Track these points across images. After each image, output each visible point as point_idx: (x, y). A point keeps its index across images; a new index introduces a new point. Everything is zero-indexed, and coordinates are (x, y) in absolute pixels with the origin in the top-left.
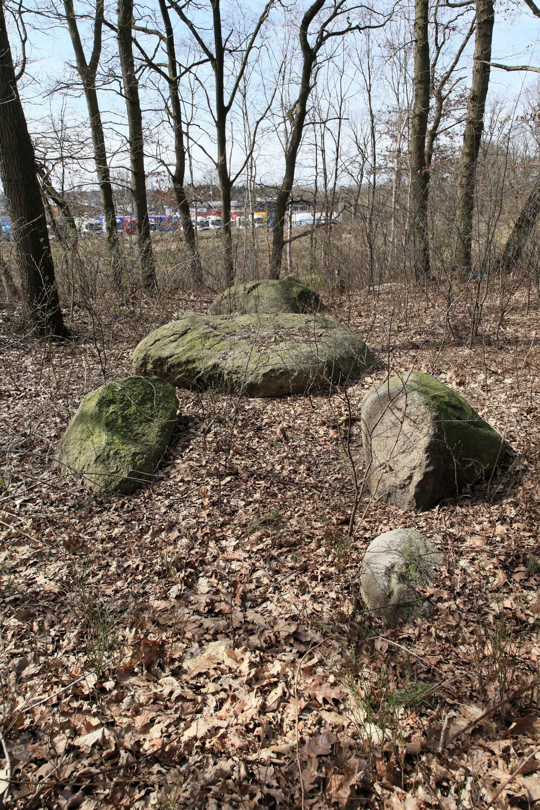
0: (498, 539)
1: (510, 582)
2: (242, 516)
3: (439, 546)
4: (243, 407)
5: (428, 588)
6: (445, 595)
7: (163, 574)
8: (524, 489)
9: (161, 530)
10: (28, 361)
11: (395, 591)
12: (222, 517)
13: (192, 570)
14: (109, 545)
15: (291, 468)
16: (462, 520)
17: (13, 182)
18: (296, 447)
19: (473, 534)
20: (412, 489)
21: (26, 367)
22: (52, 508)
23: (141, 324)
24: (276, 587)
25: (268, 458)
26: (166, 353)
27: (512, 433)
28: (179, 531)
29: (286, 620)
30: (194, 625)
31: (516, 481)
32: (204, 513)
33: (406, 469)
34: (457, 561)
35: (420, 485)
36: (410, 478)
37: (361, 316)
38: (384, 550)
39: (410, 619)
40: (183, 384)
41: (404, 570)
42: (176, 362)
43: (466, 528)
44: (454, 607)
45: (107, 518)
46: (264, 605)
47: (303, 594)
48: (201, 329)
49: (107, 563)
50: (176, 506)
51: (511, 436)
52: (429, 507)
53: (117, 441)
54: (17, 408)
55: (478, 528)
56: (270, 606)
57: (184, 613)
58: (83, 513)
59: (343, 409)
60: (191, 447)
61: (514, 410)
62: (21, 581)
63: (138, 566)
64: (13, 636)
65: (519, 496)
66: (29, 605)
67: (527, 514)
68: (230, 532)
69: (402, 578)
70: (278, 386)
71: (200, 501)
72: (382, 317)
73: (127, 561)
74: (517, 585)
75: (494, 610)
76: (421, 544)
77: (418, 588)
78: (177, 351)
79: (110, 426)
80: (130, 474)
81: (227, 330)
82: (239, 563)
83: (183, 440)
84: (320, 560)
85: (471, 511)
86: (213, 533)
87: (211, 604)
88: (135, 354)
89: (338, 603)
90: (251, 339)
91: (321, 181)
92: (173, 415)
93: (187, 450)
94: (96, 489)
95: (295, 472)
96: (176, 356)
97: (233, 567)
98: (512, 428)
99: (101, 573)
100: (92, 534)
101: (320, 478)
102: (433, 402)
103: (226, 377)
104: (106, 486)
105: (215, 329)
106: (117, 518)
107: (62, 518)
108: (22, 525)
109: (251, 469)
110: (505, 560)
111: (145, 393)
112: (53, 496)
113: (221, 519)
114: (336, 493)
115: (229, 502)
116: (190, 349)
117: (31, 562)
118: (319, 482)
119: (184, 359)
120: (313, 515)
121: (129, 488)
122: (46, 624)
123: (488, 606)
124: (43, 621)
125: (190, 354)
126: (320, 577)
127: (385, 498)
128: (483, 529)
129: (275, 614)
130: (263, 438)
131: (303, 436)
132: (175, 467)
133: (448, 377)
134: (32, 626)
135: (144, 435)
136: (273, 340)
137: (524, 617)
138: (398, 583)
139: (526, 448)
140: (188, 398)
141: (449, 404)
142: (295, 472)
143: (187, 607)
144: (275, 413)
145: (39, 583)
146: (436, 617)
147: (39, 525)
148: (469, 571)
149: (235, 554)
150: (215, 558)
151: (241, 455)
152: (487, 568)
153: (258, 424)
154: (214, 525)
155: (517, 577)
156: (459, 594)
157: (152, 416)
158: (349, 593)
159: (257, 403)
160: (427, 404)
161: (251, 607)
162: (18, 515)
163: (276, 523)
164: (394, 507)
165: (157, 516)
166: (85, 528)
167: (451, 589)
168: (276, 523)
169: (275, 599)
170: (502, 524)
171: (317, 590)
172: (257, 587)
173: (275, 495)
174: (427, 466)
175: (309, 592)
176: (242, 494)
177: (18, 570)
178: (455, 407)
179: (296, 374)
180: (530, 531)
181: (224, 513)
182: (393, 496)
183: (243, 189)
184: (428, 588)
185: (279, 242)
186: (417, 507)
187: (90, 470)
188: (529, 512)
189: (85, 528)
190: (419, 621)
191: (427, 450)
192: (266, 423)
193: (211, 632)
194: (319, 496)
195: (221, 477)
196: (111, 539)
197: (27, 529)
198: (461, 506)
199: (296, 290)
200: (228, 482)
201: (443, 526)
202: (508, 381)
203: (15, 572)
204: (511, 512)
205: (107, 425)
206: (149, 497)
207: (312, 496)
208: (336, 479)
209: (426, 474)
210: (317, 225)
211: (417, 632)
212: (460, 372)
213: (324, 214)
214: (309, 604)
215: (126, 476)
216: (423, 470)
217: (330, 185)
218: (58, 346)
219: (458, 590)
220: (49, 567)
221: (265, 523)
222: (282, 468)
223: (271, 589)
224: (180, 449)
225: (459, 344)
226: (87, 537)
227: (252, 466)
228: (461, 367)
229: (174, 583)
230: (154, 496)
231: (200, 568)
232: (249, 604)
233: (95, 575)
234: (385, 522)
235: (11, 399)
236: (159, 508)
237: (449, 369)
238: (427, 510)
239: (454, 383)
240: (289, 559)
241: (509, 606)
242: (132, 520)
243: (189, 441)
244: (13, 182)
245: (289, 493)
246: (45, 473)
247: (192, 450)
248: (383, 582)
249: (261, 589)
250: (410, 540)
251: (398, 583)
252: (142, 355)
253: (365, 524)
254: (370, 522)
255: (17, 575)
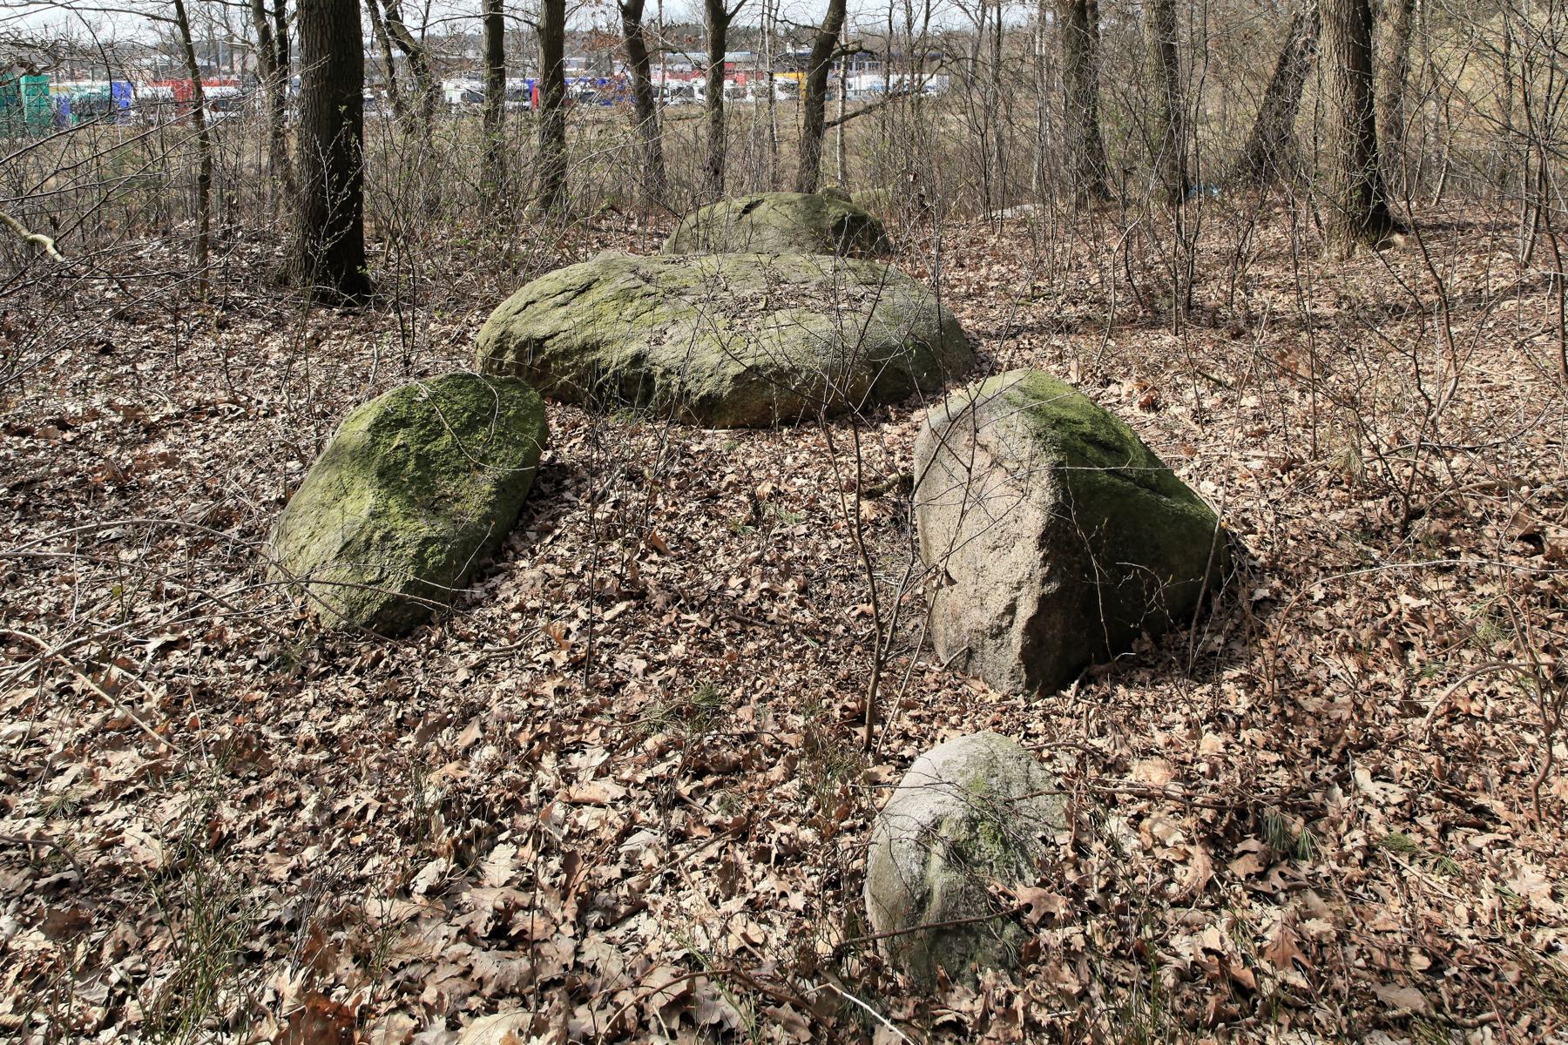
0: (1204, 767)
1: (1222, 880)
2: (634, 697)
3: (1060, 780)
4: (687, 447)
5: (1019, 886)
6: (1060, 907)
7: (414, 833)
8: (1273, 646)
9: (443, 723)
10: (274, 347)
11: (937, 889)
12: (588, 695)
13: (477, 822)
14: (316, 757)
15: (766, 585)
16: (1127, 719)
17: (316, 11)
18: (785, 538)
19: (1147, 753)
20: (1016, 637)
21: (266, 357)
22: (220, 664)
23: (512, 270)
24: (670, 876)
25: (720, 561)
26: (541, 330)
27: (1248, 515)
28: (483, 728)
29: (676, 963)
30: (455, 970)
31: (1249, 628)
32: (549, 687)
33: (1002, 588)
34: (1101, 821)
35: (1032, 626)
36: (1011, 609)
37: (962, 266)
38: (930, 787)
39: (966, 971)
40: (568, 397)
41: (963, 834)
42: (560, 347)
43: (1135, 740)
44: (1078, 942)
45: (333, 690)
46: (631, 923)
47: (728, 898)
48: (620, 280)
49: (298, 799)
50: (492, 667)
51: (1245, 521)
52: (1053, 687)
53: (395, 510)
54: (223, 439)
55: (1160, 739)
56: (644, 925)
57: (436, 937)
58: (283, 678)
59: (897, 458)
60: (557, 532)
61: (1256, 464)
62: (89, 836)
63: (365, 810)
64: (19, 979)
65: (1258, 662)
66: (75, 895)
67: (1274, 708)
68: (596, 733)
69: (958, 855)
70: (763, 402)
71: (548, 656)
72: (1004, 270)
73: (344, 795)
74: (1239, 889)
75: (1177, 955)
76: (1017, 773)
77: (996, 886)
78: (565, 326)
79: (388, 476)
80: (408, 587)
81: (672, 284)
82: (600, 812)
83: (545, 516)
84: (786, 807)
85: (1150, 697)
86: (557, 733)
87: (503, 916)
88: (485, 333)
89: (807, 923)
90: (712, 304)
91: (900, 18)
92: (532, 457)
93: (549, 539)
94: (328, 622)
95: (773, 595)
96: (562, 335)
97: (582, 821)
98: (1248, 504)
99: (275, 824)
100: (288, 728)
101: (826, 613)
102: (1052, 433)
103: (658, 381)
104: (351, 614)
105: (648, 281)
106: (355, 692)
107: (237, 685)
108: (141, 700)
109: (675, 586)
110: (1215, 821)
111: (478, 408)
112: (232, 635)
113: (584, 702)
114: (857, 648)
115: (611, 661)
116: (592, 322)
117: (130, 790)
118: (824, 620)
119: (577, 341)
120: (791, 699)
121: (399, 622)
122: (108, 950)
123: (1164, 945)
124: (102, 941)
125: (590, 330)
126: (775, 852)
127: (962, 660)
128: (1170, 743)
129: (653, 948)
130: (719, 516)
131: (803, 513)
132: (512, 577)
133: (1124, 392)
134: (70, 955)
135: (457, 500)
136: (761, 305)
137: (1247, 976)
138: (944, 870)
139: (1277, 548)
140: (575, 426)
141: (1090, 439)
142: (773, 595)
143: (448, 919)
144: (750, 462)
145: (127, 844)
146: (1032, 968)
147: (179, 703)
148: (1127, 849)
149: (593, 791)
150: (547, 796)
151: (660, 553)
152: (1170, 843)
153: (713, 485)
154: (565, 716)
155: (1240, 868)
156: (1095, 907)
157: (484, 458)
158: (837, 898)
159: (718, 438)
160: (1039, 436)
161: (601, 928)
162: (144, 676)
163: (705, 714)
164: (979, 685)
165: (445, 691)
166: (277, 713)
167: (1077, 892)
168: (705, 714)
169: (660, 908)
170: (1216, 731)
171: (763, 886)
172: (626, 874)
173: (717, 649)
174: (1046, 581)
175: (743, 891)
176: (646, 644)
177: (93, 808)
178: (1105, 447)
179: (803, 375)
180: (1279, 749)
181: (593, 687)
182: (978, 656)
183: (747, 33)
184: (1019, 886)
185: (816, 126)
186: (1030, 685)
187: (325, 576)
188: (1279, 702)
189: (277, 713)
190: (988, 977)
191: (1045, 540)
192: (730, 483)
193: (488, 991)
194: (816, 653)
195: (606, 602)
196: (327, 740)
197: (149, 711)
198: (1128, 687)
199: (834, 212)
200: (620, 615)
201: (1082, 732)
202: (1250, 401)
203: (86, 813)
204: (1240, 702)
205: (381, 474)
206: (439, 646)
207: (799, 655)
208: (863, 614)
209: (1043, 601)
210: (892, 96)
211: (978, 1007)
212: (1149, 381)
213: (907, 77)
214: (738, 925)
215: (397, 591)
216: (1037, 591)
217: (918, 25)
218: (343, 315)
219: (1093, 895)
220: (164, 803)
221: (677, 714)
222: (746, 585)
223: (657, 880)
224: (532, 535)
225: (1153, 325)
226: (277, 736)
227: (682, 579)
228: (1155, 370)
229: (434, 856)
230: (451, 641)
231: (506, 822)
232: (594, 917)
233: (260, 826)
234: (953, 719)
235: (216, 420)
236: (453, 672)
237: (1126, 375)
238: (1054, 693)
239: (1136, 404)
240: (713, 804)
241: (1216, 946)
242: (386, 698)
243: (555, 518)
244: (316, 11)
245: (751, 646)
246: (233, 582)
247: (557, 538)
248: (908, 862)
249: (633, 881)
250: (991, 763)
251: (944, 870)
252: (497, 333)
253: (906, 723)
254: (918, 719)
255: (86, 821)
